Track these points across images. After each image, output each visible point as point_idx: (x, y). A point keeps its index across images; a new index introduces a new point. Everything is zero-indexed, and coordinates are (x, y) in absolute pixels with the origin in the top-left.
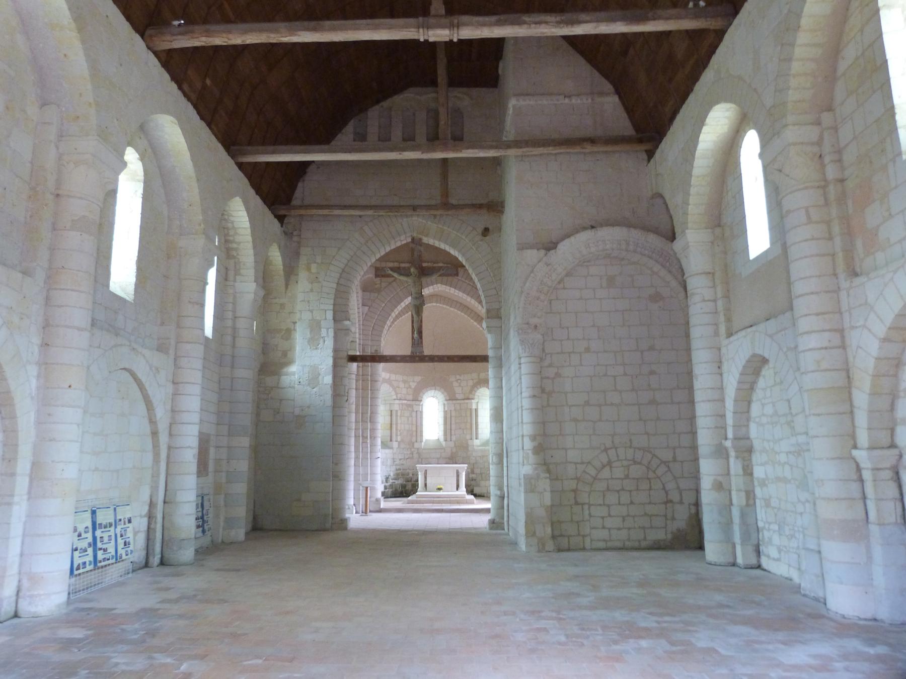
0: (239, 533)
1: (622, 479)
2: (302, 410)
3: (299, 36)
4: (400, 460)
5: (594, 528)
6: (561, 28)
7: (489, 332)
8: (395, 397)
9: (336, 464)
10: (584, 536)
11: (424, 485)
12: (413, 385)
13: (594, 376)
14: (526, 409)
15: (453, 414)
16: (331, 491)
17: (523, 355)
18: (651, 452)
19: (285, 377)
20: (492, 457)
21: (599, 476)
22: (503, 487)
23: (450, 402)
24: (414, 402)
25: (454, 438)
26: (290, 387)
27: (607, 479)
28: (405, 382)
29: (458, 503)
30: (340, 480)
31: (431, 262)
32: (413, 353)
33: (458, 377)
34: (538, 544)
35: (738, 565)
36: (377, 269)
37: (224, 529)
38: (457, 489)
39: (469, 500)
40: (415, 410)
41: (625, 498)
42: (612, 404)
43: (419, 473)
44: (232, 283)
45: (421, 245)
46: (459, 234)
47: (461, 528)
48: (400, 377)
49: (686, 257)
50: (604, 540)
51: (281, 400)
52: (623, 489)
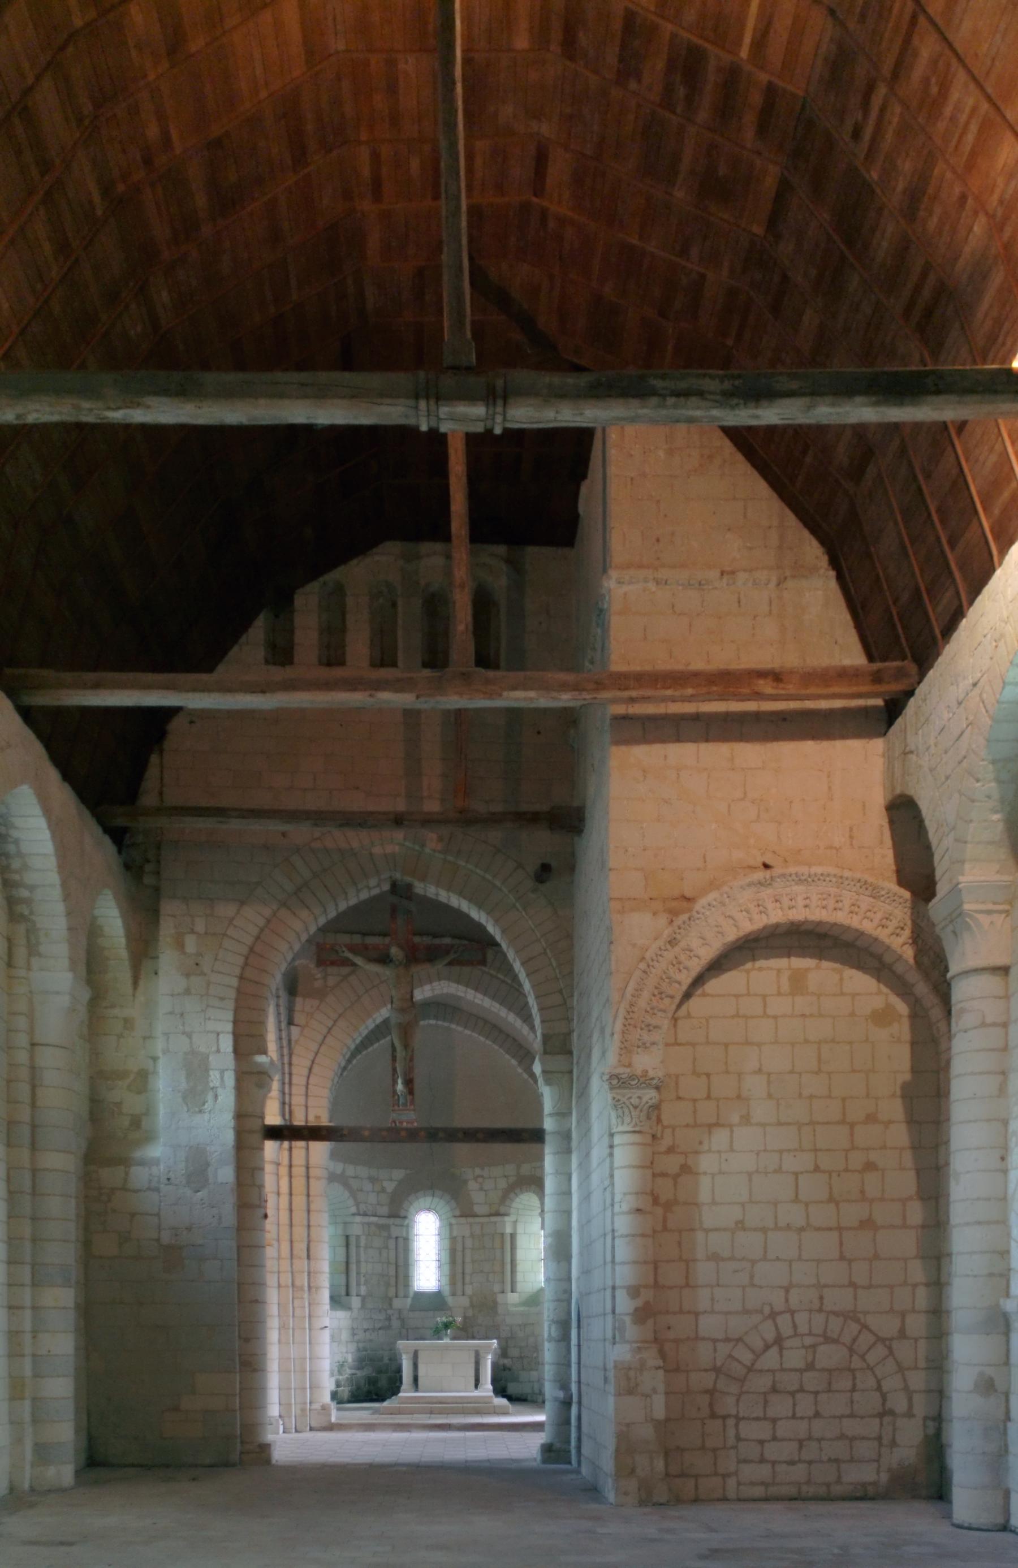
0: (65, 1473)
1: (801, 1371)
2: (176, 1235)
3: (148, 407)
4: (365, 1331)
5: (746, 1461)
6: (733, 407)
7: (548, 1082)
8: (353, 1210)
9: (247, 1340)
10: (725, 1476)
11: (411, 1379)
12: (390, 1187)
13: (757, 1171)
14: (622, 1236)
15: (469, 1243)
16: (238, 1392)
17: (621, 1128)
18: (857, 1321)
19: (140, 1168)
20: (550, 1328)
21: (758, 1366)
22: (570, 1383)
23: (463, 1220)
24: (391, 1221)
25: (469, 1290)
26: (149, 1189)
27: (773, 1371)
28: (372, 1180)
29: (478, 1412)
30: (255, 1370)
31: (428, 934)
32: (395, 1122)
33: (478, 1171)
34: (639, 1490)
35: (1013, 1529)
36: (320, 948)
37: (33, 1465)
38: (476, 1386)
39: (499, 1407)
40: (394, 1235)
41: (805, 1405)
42: (788, 1227)
43: (404, 1357)
44: (22, 973)
45: (409, 898)
46: (488, 877)
47: (489, 1461)
48: (363, 1171)
49: (954, 932)
50: (763, 1483)
51: (133, 1215)
52: (802, 1390)
